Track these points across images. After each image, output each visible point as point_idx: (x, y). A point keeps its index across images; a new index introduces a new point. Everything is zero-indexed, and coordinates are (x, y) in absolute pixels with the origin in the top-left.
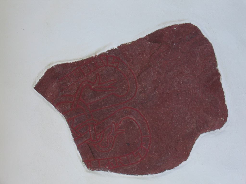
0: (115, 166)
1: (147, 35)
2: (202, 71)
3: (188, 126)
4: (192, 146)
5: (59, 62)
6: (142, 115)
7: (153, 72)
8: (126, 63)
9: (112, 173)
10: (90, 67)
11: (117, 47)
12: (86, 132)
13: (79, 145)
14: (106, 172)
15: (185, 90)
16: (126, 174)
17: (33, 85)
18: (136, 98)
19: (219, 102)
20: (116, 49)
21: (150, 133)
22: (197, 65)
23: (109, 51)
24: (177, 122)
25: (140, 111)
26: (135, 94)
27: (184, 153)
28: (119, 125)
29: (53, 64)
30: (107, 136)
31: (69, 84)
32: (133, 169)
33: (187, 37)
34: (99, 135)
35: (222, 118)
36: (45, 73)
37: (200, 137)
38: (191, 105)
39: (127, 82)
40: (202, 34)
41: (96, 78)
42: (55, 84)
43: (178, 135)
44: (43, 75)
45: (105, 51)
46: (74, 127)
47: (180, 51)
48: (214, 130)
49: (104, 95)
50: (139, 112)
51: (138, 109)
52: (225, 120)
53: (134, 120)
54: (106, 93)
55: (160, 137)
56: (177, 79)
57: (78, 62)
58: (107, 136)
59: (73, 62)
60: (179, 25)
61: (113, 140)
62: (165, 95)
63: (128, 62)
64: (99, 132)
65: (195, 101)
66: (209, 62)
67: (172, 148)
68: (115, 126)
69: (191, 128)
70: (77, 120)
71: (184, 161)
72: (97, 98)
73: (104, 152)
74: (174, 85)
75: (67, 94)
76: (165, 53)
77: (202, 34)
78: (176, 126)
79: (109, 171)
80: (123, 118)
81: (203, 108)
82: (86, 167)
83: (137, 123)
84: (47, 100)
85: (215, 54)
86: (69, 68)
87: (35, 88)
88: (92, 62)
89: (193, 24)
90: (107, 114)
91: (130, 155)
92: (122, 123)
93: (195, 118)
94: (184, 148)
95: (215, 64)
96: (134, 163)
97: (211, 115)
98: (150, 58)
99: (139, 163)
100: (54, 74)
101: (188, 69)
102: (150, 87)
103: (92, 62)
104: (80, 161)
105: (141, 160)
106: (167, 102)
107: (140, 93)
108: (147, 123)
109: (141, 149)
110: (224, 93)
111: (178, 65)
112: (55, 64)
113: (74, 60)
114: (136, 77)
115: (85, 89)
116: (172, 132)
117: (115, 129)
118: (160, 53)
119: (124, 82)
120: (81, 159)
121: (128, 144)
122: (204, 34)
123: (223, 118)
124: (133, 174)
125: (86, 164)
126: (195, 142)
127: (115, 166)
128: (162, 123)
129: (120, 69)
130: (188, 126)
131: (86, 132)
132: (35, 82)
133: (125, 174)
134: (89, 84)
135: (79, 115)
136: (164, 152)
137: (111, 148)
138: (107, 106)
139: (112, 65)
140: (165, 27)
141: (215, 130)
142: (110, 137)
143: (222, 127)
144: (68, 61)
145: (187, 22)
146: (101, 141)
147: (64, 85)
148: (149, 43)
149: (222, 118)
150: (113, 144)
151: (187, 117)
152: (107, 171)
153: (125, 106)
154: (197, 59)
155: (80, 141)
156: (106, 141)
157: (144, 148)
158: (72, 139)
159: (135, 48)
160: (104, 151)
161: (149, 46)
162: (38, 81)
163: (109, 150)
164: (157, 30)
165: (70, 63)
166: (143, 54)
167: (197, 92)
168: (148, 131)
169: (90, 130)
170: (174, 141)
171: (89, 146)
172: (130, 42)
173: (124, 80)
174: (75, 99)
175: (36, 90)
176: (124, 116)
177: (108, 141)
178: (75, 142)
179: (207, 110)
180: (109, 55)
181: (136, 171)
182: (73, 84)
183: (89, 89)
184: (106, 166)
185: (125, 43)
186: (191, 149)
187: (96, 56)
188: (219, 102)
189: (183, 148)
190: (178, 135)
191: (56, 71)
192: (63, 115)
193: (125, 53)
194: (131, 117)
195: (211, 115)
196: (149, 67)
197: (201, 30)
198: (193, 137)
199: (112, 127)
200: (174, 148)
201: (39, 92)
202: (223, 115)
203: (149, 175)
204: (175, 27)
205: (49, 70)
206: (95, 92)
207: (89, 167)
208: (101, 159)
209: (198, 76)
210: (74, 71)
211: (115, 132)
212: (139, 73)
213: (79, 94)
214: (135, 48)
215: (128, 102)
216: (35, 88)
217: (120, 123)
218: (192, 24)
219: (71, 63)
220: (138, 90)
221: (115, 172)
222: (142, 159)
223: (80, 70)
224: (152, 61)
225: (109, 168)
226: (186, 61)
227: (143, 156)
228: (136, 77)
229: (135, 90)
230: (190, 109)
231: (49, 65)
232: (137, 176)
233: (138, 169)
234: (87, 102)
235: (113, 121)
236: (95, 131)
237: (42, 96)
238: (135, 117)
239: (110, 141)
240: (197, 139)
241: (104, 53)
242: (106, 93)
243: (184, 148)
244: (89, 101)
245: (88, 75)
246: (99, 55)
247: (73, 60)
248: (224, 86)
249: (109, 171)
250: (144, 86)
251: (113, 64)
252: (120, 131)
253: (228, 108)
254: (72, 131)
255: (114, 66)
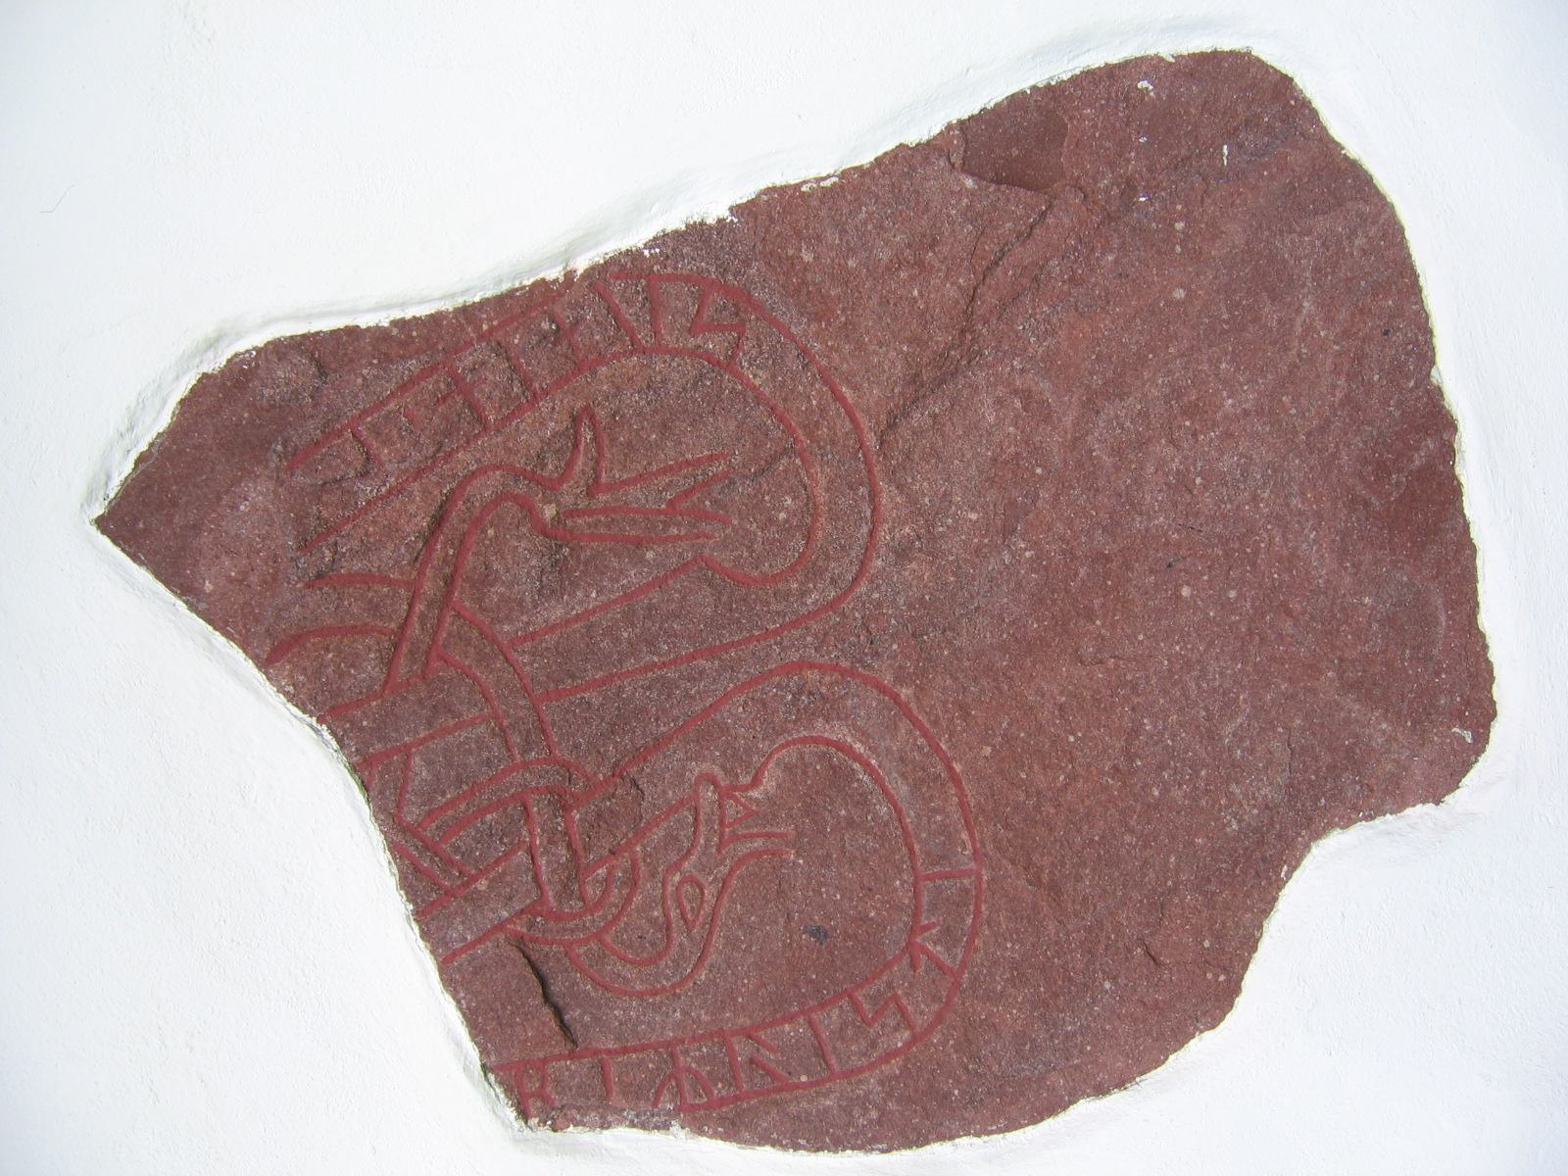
0: (720, 1090)
1: (949, 127)
2: (1339, 395)
3: (1233, 787)
4: (1260, 927)
5: (294, 317)
6: (915, 722)
7: (990, 401)
8: (793, 329)
9: (704, 1139)
10: (528, 364)
11: (731, 209)
12: (507, 855)
13: (455, 954)
14: (656, 1136)
15: (1220, 536)
16: (804, 1148)
17: (90, 498)
18: (876, 595)
19: (1443, 618)
20: (720, 221)
21: (975, 851)
22: (1304, 351)
23: (672, 243)
24: (1161, 767)
25: (905, 693)
26: (863, 565)
27: (1209, 976)
28: (751, 798)
29: (239, 336)
30: (660, 877)
31: (368, 490)
32: (856, 1112)
33: (1225, 147)
34: (602, 871)
35: (1456, 730)
36: (182, 402)
37: (1308, 862)
38: (1262, 639)
39: (803, 473)
40: (1328, 135)
41: (576, 446)
42: (257, 495)
43: (1172, 860)
44: (164, 421)
45: (637, 237)
46: (412, 814)
47: (1178, 249)
48: (1399, 806)
49: (633, 577)
50: (895, 698)
51: (888, 679)
52: (1474, 738)
53: (858, 758)
54: (650, 555)
55: (1045, 878)
56: (1170, 450)
57: (436, 319)
58: (660, 877)
59: (397, 324)
60: (1170, 64)
61: (707, 908)
62: (1082, 572)
63: (814, 327)
64: (606, 853)
65: (1289, 613)
66: (1386, 333)
67: (1129, 951)
68: (721, 806)
69: (1254, 806)
70: (429, 763)
71: (1202, 1032)
72: (580, 594)
73: (640, 995)
74: (1148, 497)
75: (357, 566)
76: (1076, 261)
77: (1324, 129)
78: (1156, 793)
79: (675, 1128)
80: (781, 740)
81: (1341, 660)
82: (511, 1114)
83: (877, 780)
84: (200, 614)
85: (1422, 281)
86: (365, 372)
87: (102, 523)
88: (545, 325)
89: (1263, 57)
90: (657, 720)
91: (835, 1013)
92: (769, 784)
93: (1280, 730)
94: (1207, 944)
95: (1423, 353)
96: (861, 1070)
97: (1387, 711)
98: (973, 299)
99: (894, 1067)
100: (246, 415)
101: (1241, 385)
102: (973, 509)
103: (545, 325)
104: (466, 1069)
105: (908, 1045)
106: (1098, 623)
107: (902, 553)
108: (954, 778)
109: (913, 966)
110: (1473, 549)
111: (1171, 350)
112: (260, 339)
113: (403, 305)
114: (871, 440)
115: (491, 532)
116: (1128, 838)
117: (722, 823)
118: (1047, 260)
119: (785, 471)
120: (473, 1053)
121: (819, 933)
122: (1337, 130)
123: (1462, 727)
124: (853, 1148)
125: (509, 1091)
126: (1275, 899)
127: (724, 1093)
128: (1062, 778)
129: (755, 376)
130: (1233, 787)
131: (507, 855)
132: (103, 478)
133: (796, 1147)
134: (521, 488)
135: (451, 723)
136: (1070, 979)
137: (696, 967)
138: (656, 659)
139: (692, 342)
140: (1077, 72)
141: (1409, 811)
142: (681, 882)
143: (1457, 792)
144: (353, 312)
145: (1227, 44)
146: (617, 918)
147: (325, 498)
148: (969, 183)
149: (1456, 730)
150: (710, 933)
151: (1229, 729)
152: (665, 1126)
153: (795, 657)
154: (1298, 311)
155: (460, 928)
156: (656, 913)
157: (930, 956)
158: (395, 906)
159: (863, 216)
160: (638, 987)
161: (969, 207)
162: (128, 467)
163: (677, 979)
164: (1023, 92)
165: (369, 329)
166: (920, 263)
167: (1304, 546)
168: (965, 836)
169: (531, 833)
170: (1141, 901)
171: (528, 958)
172: (829, 176)
173: (784, 461)
174: (411, 606)
175: (115, 541)
176: (790, 726)
177: (666, 915)
178: (425, 935)
179: (1364, 671)
180: (669, 270)
181: (879, 1122)
182: (397, 490)
183: (524, 530)
184: (658, 1094)
185: (792, 182)
186: (1251, 944)
187: (569, 275)
188: (1443, 618)
189: (1201, 943)
190: (1172, 860)
191: (266, 392)
192: (329, 728)
193: (791, 252)
194: (839, 732)
195: (1387, 711)
196: (964, 362)
197: (1318, 104)
198: (1264, 859)
199: (696, 810)
200: (1139, 950)
201: (134, 558)
202: (1467, 703)
203: (964, 1141)
204: (1146, 76)
205: (205, 384)
206: (566, 551)
207: (533, 1111)
208: (625, 1050)
209: (1309, 434)
210: (403, 387)
211: (719, 851)
212: (896, 406)
213: (447, 571)
214: (863, 216)
215: (814, 626)
216: (102, 523)
217: (756, 782)
218: (1258, 60)
219: (378, 327)
220: (884, 535)
221: (726, 1137)
222: (915, 1039)
223: (448, 385)
224: (986, 322)
225: (678, 1110)
226: (1227, 322)
227: (922, 1013)
228: (871, 440)
229: (865, 530)
230: (1249, 668)
231: (213, 344)
232: (886, 1156)
233: (891, 1105)
234: (506, 628)
235: (705, 767)
236: (569, 846)
237: (160, 587)
238: (864, 735)
239: (683, 916)
240: (1289, 875)
241: (633, 255)
242: (650, 555)
243: (1207, 944)
244: (525, 618)
245: (509, 418)
246: (589, 273)
247: (440, 299)
248: (1476, 505)
249: (675, 1128)
250: (927, 500)
251: (699, 341)
252: (758, 843)
253: (1494, 655)
254: (395, 849)
255: (706, 351)
